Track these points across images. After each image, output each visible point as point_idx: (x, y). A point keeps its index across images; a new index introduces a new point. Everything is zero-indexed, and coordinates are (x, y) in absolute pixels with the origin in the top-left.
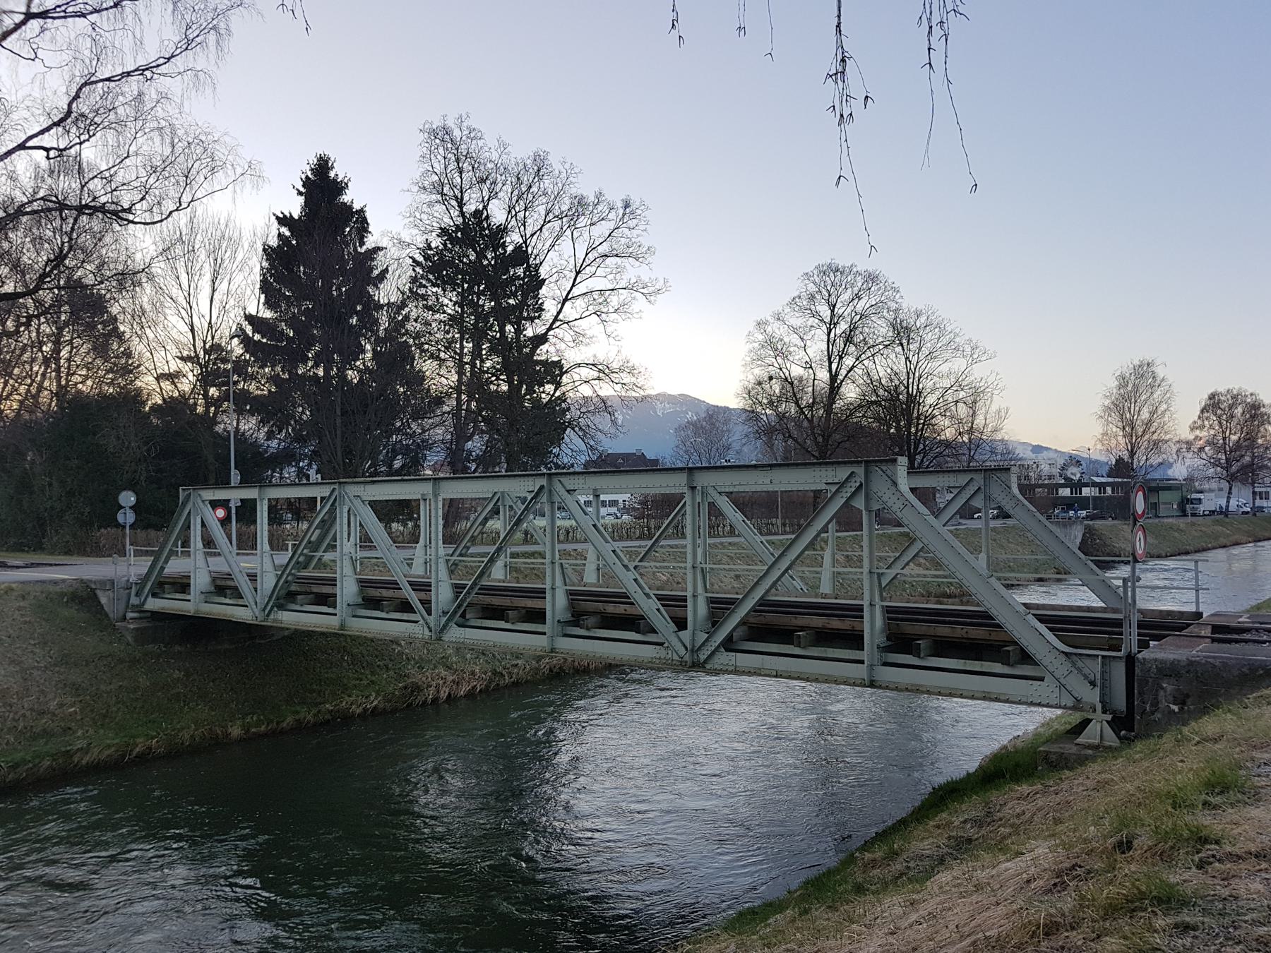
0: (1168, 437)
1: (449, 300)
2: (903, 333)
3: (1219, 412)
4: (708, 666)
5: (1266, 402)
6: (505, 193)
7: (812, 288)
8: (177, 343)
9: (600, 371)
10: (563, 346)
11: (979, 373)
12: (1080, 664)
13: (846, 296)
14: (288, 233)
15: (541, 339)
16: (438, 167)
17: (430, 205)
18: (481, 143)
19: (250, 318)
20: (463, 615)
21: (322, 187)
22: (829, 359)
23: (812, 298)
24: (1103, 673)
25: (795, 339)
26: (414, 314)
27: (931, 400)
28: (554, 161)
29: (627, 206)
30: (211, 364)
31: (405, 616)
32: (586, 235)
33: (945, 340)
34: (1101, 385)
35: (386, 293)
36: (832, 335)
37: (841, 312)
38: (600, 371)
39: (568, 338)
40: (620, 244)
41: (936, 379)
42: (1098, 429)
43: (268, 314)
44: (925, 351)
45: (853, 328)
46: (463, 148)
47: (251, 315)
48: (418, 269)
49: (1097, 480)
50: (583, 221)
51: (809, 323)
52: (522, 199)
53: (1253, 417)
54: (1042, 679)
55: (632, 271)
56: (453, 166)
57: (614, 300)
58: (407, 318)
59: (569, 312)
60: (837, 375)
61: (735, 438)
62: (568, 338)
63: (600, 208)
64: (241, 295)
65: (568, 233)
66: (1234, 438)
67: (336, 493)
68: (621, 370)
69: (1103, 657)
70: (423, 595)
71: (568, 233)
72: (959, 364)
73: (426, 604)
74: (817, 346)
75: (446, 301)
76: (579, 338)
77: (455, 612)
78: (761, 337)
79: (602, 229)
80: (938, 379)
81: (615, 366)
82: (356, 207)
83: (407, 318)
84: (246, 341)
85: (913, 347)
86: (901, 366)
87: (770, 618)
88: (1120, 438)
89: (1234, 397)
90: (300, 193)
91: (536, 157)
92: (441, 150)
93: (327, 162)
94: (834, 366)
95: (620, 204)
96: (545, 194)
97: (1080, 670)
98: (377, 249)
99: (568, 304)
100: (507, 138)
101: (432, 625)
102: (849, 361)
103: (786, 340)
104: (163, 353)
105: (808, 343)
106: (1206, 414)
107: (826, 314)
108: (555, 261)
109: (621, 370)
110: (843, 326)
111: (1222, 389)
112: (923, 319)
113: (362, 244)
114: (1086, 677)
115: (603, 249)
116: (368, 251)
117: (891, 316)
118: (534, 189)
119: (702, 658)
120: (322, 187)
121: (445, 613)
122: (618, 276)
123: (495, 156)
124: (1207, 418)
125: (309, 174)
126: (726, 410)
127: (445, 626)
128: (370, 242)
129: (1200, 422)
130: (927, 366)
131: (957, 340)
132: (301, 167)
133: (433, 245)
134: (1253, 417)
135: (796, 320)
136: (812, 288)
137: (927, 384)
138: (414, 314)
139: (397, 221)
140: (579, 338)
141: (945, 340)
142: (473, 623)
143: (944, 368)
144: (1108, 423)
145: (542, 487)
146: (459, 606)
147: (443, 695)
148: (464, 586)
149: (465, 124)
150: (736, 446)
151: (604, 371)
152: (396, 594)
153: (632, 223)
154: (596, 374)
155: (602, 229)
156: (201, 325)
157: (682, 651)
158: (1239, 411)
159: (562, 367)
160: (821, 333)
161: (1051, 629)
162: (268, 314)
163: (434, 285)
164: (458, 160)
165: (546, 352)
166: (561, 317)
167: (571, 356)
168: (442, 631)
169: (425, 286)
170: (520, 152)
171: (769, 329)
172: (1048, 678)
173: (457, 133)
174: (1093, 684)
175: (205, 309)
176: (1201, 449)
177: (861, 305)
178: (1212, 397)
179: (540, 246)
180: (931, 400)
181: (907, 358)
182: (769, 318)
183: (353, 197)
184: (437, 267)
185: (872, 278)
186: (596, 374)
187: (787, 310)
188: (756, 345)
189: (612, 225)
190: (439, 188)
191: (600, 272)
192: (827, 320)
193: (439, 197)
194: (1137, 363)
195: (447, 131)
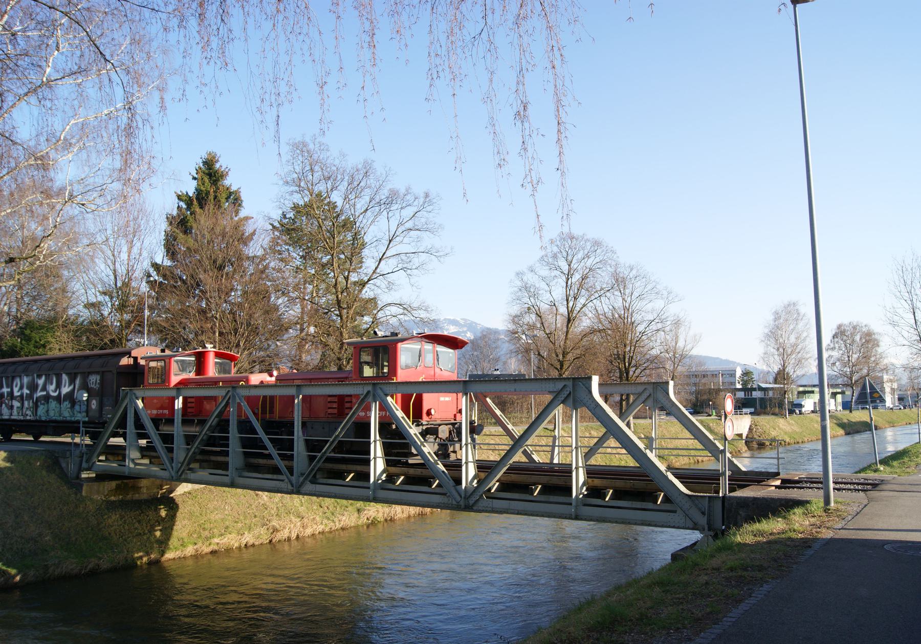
0: (809, 355)
1: (296, 255)
2: (619, 282)
3: (845, 338)
4: (475, 508)
5: (875, 331)
6: (343, 187)
7: (555, 249)
8: (103, 283)
9: (404, 309)
10: (379, 291)
11: (673, 310)
12: (697, 502)
13: (580, 255)
14: (184, 206)
15: (363, 284)
16: (298, 169)
17: (292, 193)
18: (328, 154)
19: (156, 266)
20: (314, 476)
21: (210, 172)
22: (567, 300)
23: (555, 256)
24: (709, 507)
25: (543, 285)
26: (272, 264)
27: (640, 328)
28: (379, 168)
29: (427, 195)
30: (122, 294)
31: (275, 477)
32: (398, 216)
33: (649, 287)
34: (762, 320)
35: (255, 249)
36: (569, 282)
37: (575, 266)
38: (404, 309)
39: (383, 286)
40: (420, 221)
41: (643, 314)
42: (760, 349)
43: (168, 263)
44: (636, 294)
45: (584, 278)
46: (315, 157)
47: (156, 264)
48: (276, 233)
49: (764, 385)
50: (394, 207)
51: (553, 274)
52: (354, 188)
53: (868, 342)
54: (675, 512)
55: (428, 240)
56: (308, 168)
57: (416, 261)
58: (266, 267)
59: (384, 267)
60: (572, 311)
61: (502, 353)
62: (383, 286)
63: (408, 197)
64: (151, 249)
65: (385, 213)
66: (855, 356)
67: (230, 394)
68: (419, 308)
69: (709, 497)
70: (287, 463)
71: (385, 213)
72: (659, 304)
73: (291, 470)
74: (559, 292)
75: (295, 255)
76: (390, 286)
77: (309, 474)
78: (519, 283)
79: (408, 212)
80: (644, 313)
81: (415, 305)
82: (234, 188)
83: (266, 267)
84: (152, 284)
85: (627, 291)
86: (619, 303)
87: (514, 477)
88: (776, 357)
89: (854, 328)
90: (194, 178)
91: (366, 162)
92: (300, 157)
93: (214, 157)
94: (571, 304)
95: (422, 195)
96: (370, 187)
97: (696, 506)
98: (247, 218)
99: (383, 262)
100: (345, 149)
101: (294, 482)
102: (582, 301)
103: (537, 286)
104: (93, 291)
105: (553, 288)
106: (836, 340)
107: (565, 268)
108: (375, 231)
109: (419, 308)
110: (576, 277)
111: (846, 321)
112: (634, 272)
113: (237, 213)
114: (700, 509)
115: (409, 225)
116: (241, 220)
117: (612, 270)
118: (362, 184)
119: (471, 502)
120: (210, 172)
121: (302, 474)
122: (419, 244)
123: (337, 162)
124: (837, 342)
125: (201, 165)
126: (496, 332)
127: (303, 483)
128: (243, 213)
129: (832, 345)
130: (637, 305)
131: (658, 287)
132: (194, 162)
133: (288, 216)
134: (868, 342)
135: (544, 272)
136: (555, 249)
137: (637, 317)
138: (272, 264)
139: (262, 201)
140: (390, 286)
141: (649, 287)
142: (321, 481)
143: (649, 306)
144: (768, 345)
145: (368, 392)
146: (313, 469)
147: (294, 536)
148: (315, 457)
149: (317, 140)
150: (503, 359)
151: (407, 309)
152: (269, 462)
153: (429, 209)
154: (401, 311)
155: (408, 212)
156: (122, 270)
157: (458, 498)
158: (857, 338)
159: (376, 303)
160: (562, 281)
161: (682, 482)
162: (168, 263)
163: (287, 244)
164: (311, 165)
165: (367, 293)
166: (378, 271)
167: (384, 299)
168: (300, 486)
169: (281, 245)
170: (354, 160)
171: (525, 278)
172: (679, 511)
173: (311, 146)
174: (703, 513)
175: (124, 256)
176: (834, 364)
177: (589, 263)
178: (839, 327)
179: (365, 221)
180: (640, 328)
181: (623, 299)
182: (526, 271)
183: (231, 182)
184: (288, 230)
185: (597, 244)
186: (401, 311)
187: (538, 265)
188: (516, 289)
189: (415, 209)
190: (297, 182)
191: (406, 240)
192: (566, 272)
193: (297, 188)
194: (786, 303)
195: (305, 144)
